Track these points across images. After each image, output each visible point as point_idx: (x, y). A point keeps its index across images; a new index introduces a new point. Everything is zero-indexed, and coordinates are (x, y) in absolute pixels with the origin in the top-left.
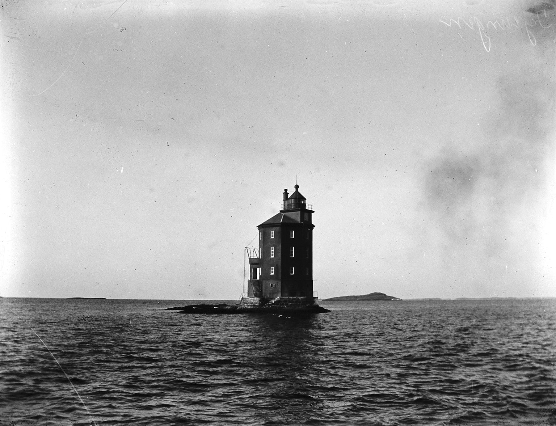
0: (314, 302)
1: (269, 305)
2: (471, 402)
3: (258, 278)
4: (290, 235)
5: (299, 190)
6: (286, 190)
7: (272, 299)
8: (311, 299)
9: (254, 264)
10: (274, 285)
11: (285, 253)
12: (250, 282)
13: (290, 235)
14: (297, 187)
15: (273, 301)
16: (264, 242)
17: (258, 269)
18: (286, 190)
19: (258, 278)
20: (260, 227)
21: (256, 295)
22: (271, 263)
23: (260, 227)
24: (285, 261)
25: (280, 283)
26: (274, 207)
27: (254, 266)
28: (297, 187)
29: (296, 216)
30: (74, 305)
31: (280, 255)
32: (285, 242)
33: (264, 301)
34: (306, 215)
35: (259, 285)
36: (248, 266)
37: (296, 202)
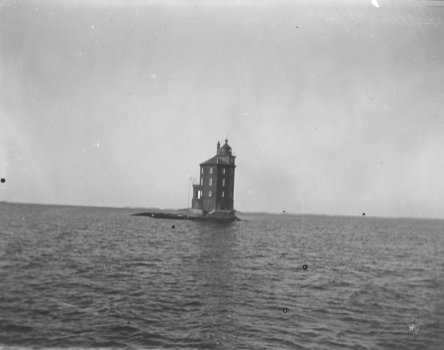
0: (234, 214)
1: (208, 216)
2: (120, 320)
3: (199, 197)
4: (220, 171)
5: (228, 143)
6: (219, 143)
7: (209, 211)
8: (233, 212)
9: (196, 188)
10: (211, 203)
11: (219, 183)
12: (193, 200)
13: (220, 171)
14: (226, 141)
15: (211, 213)
16: (204, 176)
17: (199, 192)
18: (219, 143)
19: (199, 197)
20: (202, 165)
21: (200, 209)
22: (210, 188)
23: (202, 165)
24: (219, 188)
25: (215, 202)
26: (211, 153)
27: (196, 190)
28: (226, 141)
29: (226, 160)
30: (246, 244)
31: (216, 184)
32: (219, 177)
33: (205, 213)
34: (232, 159)
35: (200, 202)
36: (192, 189)
37: (226, 151)
